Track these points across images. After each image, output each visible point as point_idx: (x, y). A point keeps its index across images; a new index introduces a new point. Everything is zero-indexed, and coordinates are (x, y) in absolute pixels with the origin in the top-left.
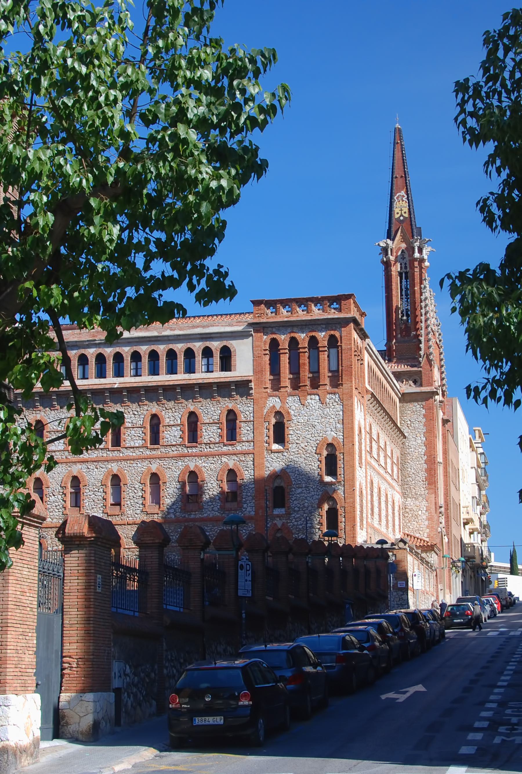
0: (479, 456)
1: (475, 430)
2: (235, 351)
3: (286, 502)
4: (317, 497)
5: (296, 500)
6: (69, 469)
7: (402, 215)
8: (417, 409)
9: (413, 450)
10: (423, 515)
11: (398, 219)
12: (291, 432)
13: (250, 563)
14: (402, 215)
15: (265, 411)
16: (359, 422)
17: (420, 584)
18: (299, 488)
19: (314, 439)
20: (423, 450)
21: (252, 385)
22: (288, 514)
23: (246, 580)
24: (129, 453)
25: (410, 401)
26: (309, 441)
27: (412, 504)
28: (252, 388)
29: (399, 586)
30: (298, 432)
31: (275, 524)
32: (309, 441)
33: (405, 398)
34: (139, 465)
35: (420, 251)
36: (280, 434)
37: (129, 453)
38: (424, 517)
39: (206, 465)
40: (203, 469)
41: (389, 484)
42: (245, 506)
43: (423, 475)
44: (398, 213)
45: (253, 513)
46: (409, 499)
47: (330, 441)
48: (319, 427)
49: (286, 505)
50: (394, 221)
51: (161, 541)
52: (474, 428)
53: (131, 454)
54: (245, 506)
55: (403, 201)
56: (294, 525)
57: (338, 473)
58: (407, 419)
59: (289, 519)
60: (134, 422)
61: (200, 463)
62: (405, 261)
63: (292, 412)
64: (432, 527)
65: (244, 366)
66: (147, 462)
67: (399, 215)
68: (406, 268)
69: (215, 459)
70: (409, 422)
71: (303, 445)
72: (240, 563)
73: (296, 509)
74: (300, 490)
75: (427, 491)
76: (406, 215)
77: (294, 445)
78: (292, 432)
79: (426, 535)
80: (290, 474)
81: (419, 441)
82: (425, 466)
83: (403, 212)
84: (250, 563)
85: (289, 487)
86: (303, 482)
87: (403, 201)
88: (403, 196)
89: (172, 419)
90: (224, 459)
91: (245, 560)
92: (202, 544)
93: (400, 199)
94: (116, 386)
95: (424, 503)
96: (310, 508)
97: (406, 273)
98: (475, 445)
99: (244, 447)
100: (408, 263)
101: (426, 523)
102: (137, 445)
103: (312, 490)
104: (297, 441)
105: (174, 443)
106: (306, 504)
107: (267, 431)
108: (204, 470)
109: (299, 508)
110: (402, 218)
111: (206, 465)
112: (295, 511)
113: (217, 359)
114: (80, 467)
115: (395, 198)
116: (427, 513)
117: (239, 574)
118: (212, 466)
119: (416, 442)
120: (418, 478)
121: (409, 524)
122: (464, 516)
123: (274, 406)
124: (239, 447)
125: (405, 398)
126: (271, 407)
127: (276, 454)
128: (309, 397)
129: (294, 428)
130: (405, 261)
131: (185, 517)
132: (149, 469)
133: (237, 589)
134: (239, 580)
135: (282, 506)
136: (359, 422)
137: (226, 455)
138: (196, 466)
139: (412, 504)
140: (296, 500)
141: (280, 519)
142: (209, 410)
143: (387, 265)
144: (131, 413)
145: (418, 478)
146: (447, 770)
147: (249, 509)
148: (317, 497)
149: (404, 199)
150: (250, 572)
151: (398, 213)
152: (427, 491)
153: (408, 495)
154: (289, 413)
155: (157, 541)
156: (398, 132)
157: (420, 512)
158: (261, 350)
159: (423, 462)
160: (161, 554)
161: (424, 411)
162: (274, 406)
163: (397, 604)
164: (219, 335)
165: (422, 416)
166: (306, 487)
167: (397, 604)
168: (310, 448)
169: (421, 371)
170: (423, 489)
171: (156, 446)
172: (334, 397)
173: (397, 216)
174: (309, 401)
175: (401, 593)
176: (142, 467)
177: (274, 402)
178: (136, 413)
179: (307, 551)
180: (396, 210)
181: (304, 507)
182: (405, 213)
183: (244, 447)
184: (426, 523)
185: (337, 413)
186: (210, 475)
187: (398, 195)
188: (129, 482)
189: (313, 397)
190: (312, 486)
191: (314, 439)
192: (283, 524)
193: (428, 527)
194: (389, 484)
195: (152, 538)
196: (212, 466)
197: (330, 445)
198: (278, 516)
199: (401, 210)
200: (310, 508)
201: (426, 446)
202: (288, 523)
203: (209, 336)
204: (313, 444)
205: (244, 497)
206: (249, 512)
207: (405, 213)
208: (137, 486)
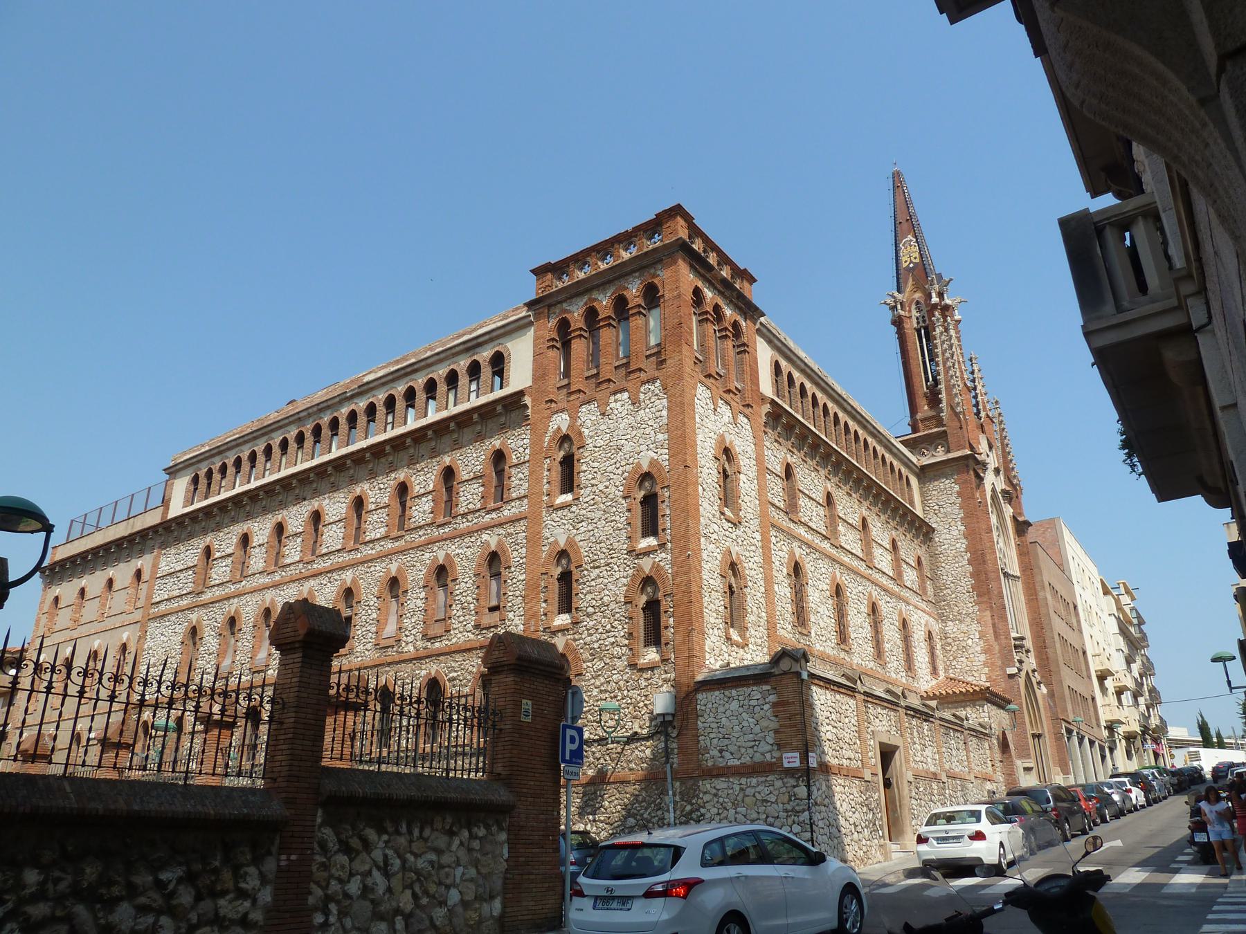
4: (625, 581)
8: (947, 491)
10: (975, 646)
11: (908, 269)
12: (584, 467)
19: (619, 471)
20: (962, 544)
21: (527, 400)
25: (936, 478)
26: (612, 476)
28: (526, 406)
29: (786, 765)
30: (596, 464)
32: (612, 476)
33: (925, 474)
35: (941, 295)
38: (978, 649)
43: (967, 583)
47: (645, 468)
48: (628, 447)
50: (901, 271)
54: (511, 615)
57: (660, 528)
58: (932, 503)
61: (452, 548)
63: (587, 432)
64: (993, 664)
68: (924, 321)
71: (601, 487)
73: (590, 610)
75: (977, 608)
76: (917, 260)
78: (585, 471)
79: (984, 678)
82: (970, 568)
86: (602, 556)
95: (975, 626)
97: (926, 328)
99: (514, 510)
101: (983, 657)
102: (378, 536)
107: (550, 472)
108: (457, 560)
113: (486, 371)
119: (951, 535)
120: (960, 589)
122: (1095, 666)
123: (559, 428)
125: (925, 474)
127: (559, 513)
128: (612, 399)
137: (487, 529)
143: (898, 322)
145: (960, 589)
148: (625, 581)
152: (977, 608)
154: (580, 434)
156: (897, 176)
157: (970, 642)
161: (957, 488)
162: (559, 428)
163: (786, 811)
164: (487, 337)
167: (786, 811)
169: (945, 432)
173: (905, 265)
174: (613, 405)
175: (792, 782)
177: (561, 422)
183: (514, 510)
184: (983, 657)
185: (658, 414)
186: (464, 568)
188: (363, 597)
191: (619, 471)
193: (985, 664)
197: (646, 476)
200: (613, 606)
203: (474, 342)
204: (618, 480)
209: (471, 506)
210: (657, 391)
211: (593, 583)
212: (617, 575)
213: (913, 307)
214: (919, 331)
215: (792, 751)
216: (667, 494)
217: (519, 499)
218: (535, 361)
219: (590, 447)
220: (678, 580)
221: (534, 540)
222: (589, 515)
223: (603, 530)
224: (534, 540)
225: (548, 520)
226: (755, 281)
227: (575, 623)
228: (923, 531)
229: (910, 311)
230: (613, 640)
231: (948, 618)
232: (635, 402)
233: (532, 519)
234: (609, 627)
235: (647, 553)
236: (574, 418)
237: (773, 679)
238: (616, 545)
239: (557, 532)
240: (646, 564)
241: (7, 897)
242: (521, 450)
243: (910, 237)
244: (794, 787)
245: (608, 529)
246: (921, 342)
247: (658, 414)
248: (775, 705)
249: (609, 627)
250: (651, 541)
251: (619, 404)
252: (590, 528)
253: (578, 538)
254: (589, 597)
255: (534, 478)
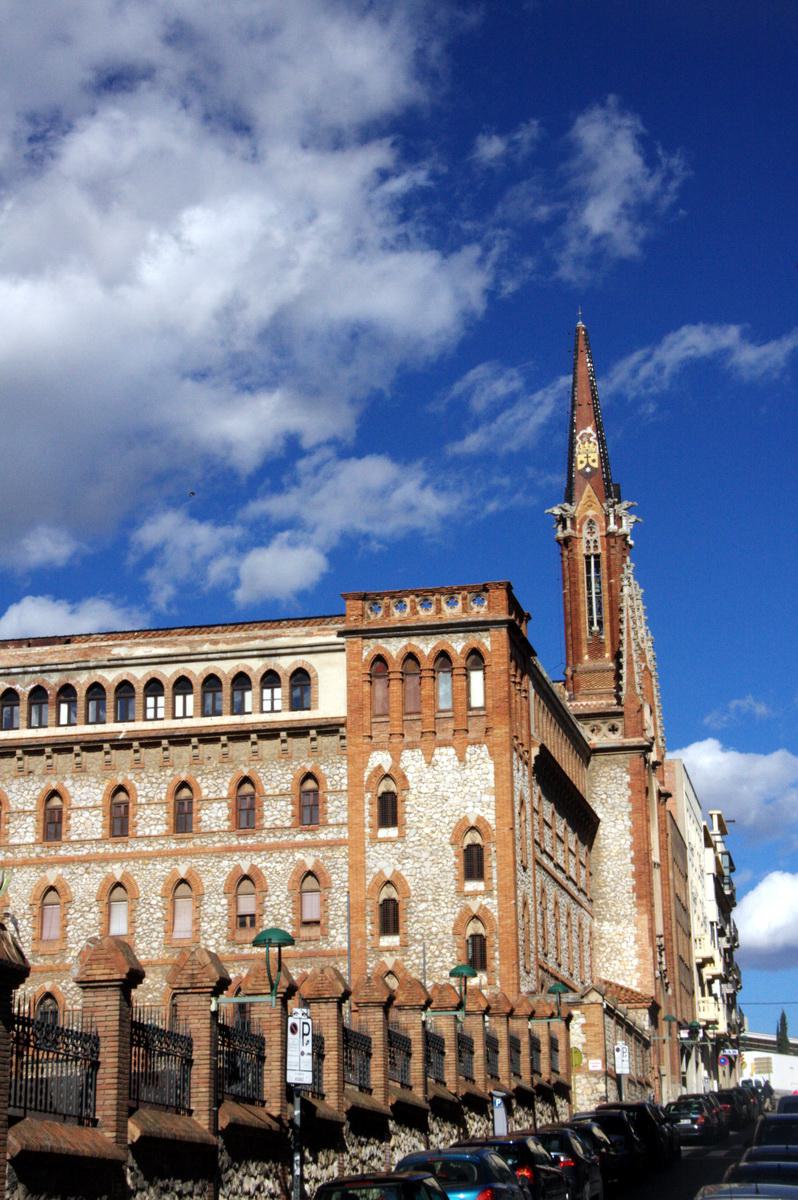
0: (720, 856)
1: (711, 815)
2: (316, 676)
3: (400, 925)
4: (453, 917)
5: (417, 921)
6: (42, 875)
7: (588, 465)
9: (610, 841)
11: (582, 472)
13: (309, 1021)
14: (588, 465)
15: (367, 774)
16: (521, 792)
17: (626, 1064)
18: (422, 901)
20: (627, 841)
22: (405, 945)
23: (302, 1054)
24: (142, 847)
27: (611, 931)
31: (383, 962)
32: (438, 822)
34: (158, 867)
36: (389, 811)
37: (142, 847)
38: (633, 953)
39: (269, 865)
40: (264, 871)
41: (573, 897)
42: (333, 932)
43: (631, 882)
44: (582, 462)
45: (345, 945)
46: (606, 923)
49: (401, 931)
51: (124, 976)
52: (711, 812)
53: (145, 849)
54: (333, 932)
55: (590, 442)
56: (414, 964)
59: (405, 954)
60: (150, 795)
62: (594, 537)
65: (331, 699)
66: (171, 861)
67: (584, 465)
69: (283, 855)
70: (604, 796)
72: (291, 1021)
73: (418, 937)
74: (423, 906)
75: (636, 910)
77: (414, 831)
78: (412, 808)
79: (635, 983)
80: (407, 878)
81: (622, 828)
83: (590, 460)
84: (309, 1021)
85: (405, 901)
86: (429, 892)
87: (590, 442)
88: (590, 435)
89: (213, 789)
90: (299, 856)
91: (300, 1015)
92: (214, 984)
93: (585, 439)
94: (121, 736)
96: (441, 936)
98: (714, 839)
100: (598, 540)
101: (636, 962)
102: (154, 833)
103: (443, 904)
104: (419, 825)
105: (215, 829)
106: (434, 930)
107: (369, 810)
109: (422, 935)
110: (588, 470)
111: (269, 865)
112: (415, 941)
114: (60, 871)
115: (578, 438)
116: (636, 946)
117: (290, 1041)
118: (279, 867)
121: (607, 965)
124: (324, 835)
126: (375, 768)
127: (384, 846)
129: (413, 803)
130: (594, 537)
131: (233, 952)
132: (175, 872)
133: (284, 1069)
134: (289, 1053)
135: (395, 931)
136: (521, 792)
138: (253, 867)
139: (611, 931)
140: (417, 921)
141: (392, 955)
142: (274, 774)
144: (146, 780)
146: (794, 754)
147: (340, 938)
148: (453, 917)
149: (591, 439)
150: (310, 1037)
151: (582, 462)
153: (604, 916)
155: (117, 976)
157: (624, 945)
158: (359, 675)
159: (629, 860)
160: (126, 998)
162: (380, 767)
163: (590, 1100)
165: (625, 786)
166: (434, 900)
167: (590, 1100)
168: (440, 835)
170: (628, 906)
171: (186, 835)
172: (478, 751)
173: (580, 467)
175: (594, 1080)
176: (162, 869)
178: (154, 780)
179: (423, 1002)
180: (580, 457)
181: (431, 933)
182: (594, 461)
184: (636, 962)
185: (484, 776)
187: (581, 433)
189: (443, 750)
190: (442, 898)
191: (447, 820)
192: (396, 963)
193: (638, 969)
194: (573, 897)
195: (107, 971)
196: (279, 867)
198: (389, 950)
199: (587, 457)
200: (441, 936)
201: (632, 834)
202: (404, 960)
205: (331, 917)
206: (341, 943)
207: (594, 461)
208: (154, 902)
209: (278, 822)
210: (482, 755)
211: (420, 915)
212: (445, 910)
213: (585, 526)
214: (588, 557)
215: (596, 1058)
216: (493, 849)
217: (338, 825)
218: (349, 691)
219: (414, 792)
220: (503, 923)
221: (357, 868)
222: (416, 854)
223: (429, 870)
224: (357, 868)
225: (371, 852)
226: (529, 617)
227: (405, 945)
228: (584, 823)
229: (580, 531)
230: (441, 964)
231: (604, 918)
232: (462, 759)
233: (356, 850)
234: (437, 953)
235: (475, 894)
236: (396, 758)
237: (583, 1007)
238: (443, 885)
239: (382, 860)
240: (474, 906)
241: (666, 1130)
242: (337, 778)
243: (589, 430)
244: (596, 1084)
245: (435, 870)
246: (589, 572)
247: (484, 776)
248: (583, 1026)
249: (437, 953)
250: (479, 886)
251: (446, 756)
252: (417, 865)
253: (404, 873)
254: (417, 926)
255: (354, 807)
